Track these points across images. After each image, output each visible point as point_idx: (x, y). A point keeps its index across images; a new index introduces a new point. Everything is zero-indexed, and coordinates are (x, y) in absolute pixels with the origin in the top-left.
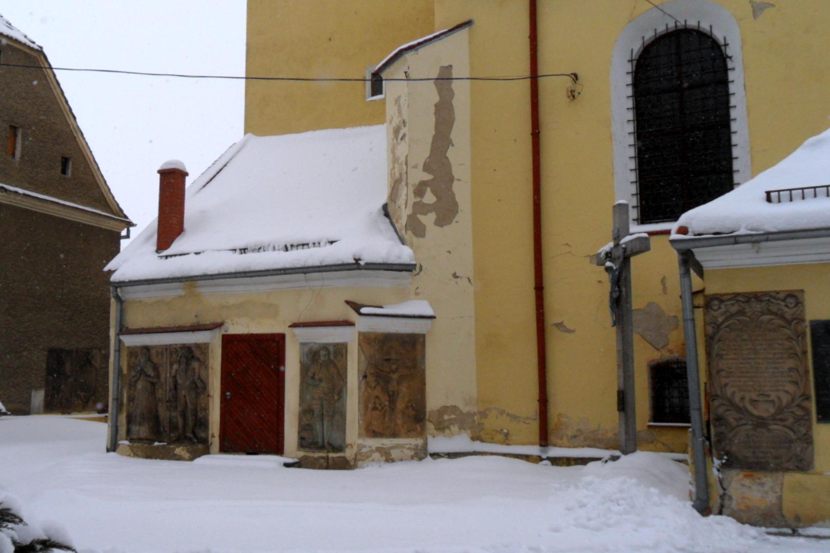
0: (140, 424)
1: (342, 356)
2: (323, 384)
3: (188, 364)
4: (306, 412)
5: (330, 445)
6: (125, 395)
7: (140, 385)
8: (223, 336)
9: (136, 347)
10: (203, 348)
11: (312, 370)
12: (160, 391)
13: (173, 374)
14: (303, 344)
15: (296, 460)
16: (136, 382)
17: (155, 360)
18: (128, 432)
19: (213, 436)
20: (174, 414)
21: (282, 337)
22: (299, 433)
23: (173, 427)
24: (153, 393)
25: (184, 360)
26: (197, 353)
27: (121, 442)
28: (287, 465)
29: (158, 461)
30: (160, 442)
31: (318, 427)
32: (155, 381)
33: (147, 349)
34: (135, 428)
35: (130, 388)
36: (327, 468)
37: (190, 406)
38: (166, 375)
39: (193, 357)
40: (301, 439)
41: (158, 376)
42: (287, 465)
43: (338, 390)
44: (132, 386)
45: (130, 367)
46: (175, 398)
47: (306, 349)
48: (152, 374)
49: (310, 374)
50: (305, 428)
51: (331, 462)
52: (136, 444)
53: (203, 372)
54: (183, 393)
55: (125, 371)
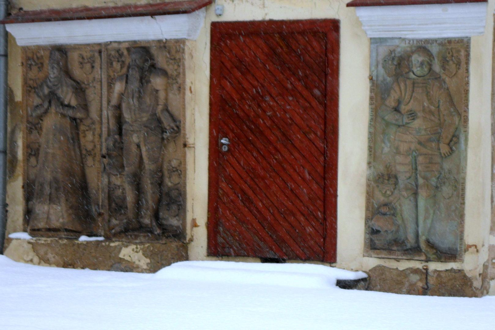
0: (51, 200)
1: (458, 64)
2: (417, 123)
3: (143, 80)
4: (382, 178)
5: (430, 245)
6: (20, 143)
7: (50, 122)
8: (215, 26)
9: (39, 48)
10: (174, 49)
11: (394, 95)
12: (90, 137)
13: (114, 102)
14: (376, 42)
15: (361, 275)
16: (40, 118)
17: (77, 72)
18: (28, 212)
19: (195, 225)
20: (117, 181)
21: (333, 25)
22: (368, 219)
23: (116, 206)
24: (76, 138)
25: (135, 74)
26: (161, 60)
27: (13, 236)
28: (343, 284)
29: (87, 272)
30: (90, 236)
31: (406, 208)
32: (79, 115)
33: (61, 51)
34: (41, 209)
35: (30, 131)
36: (425, 291)
37: (149, 166)
38: (100, 108)
39: (153, 66)
40: (372, 232)
41: (85, 107)
42: (343, 284)
43: (449, 136)
44: (34, 126)
45: (30, 88)
46: (120, 147)
47: (383, 50)
48: (74, 103)
49: (391, 102)
50: (378, 211)
51: (432, 281)
52: (43, 240)
53: (174, 98)
54: (135, 138)
55: (19, 96)
